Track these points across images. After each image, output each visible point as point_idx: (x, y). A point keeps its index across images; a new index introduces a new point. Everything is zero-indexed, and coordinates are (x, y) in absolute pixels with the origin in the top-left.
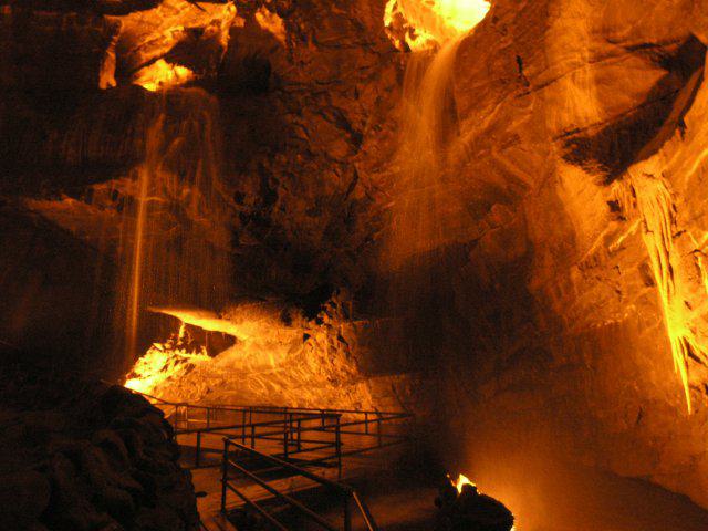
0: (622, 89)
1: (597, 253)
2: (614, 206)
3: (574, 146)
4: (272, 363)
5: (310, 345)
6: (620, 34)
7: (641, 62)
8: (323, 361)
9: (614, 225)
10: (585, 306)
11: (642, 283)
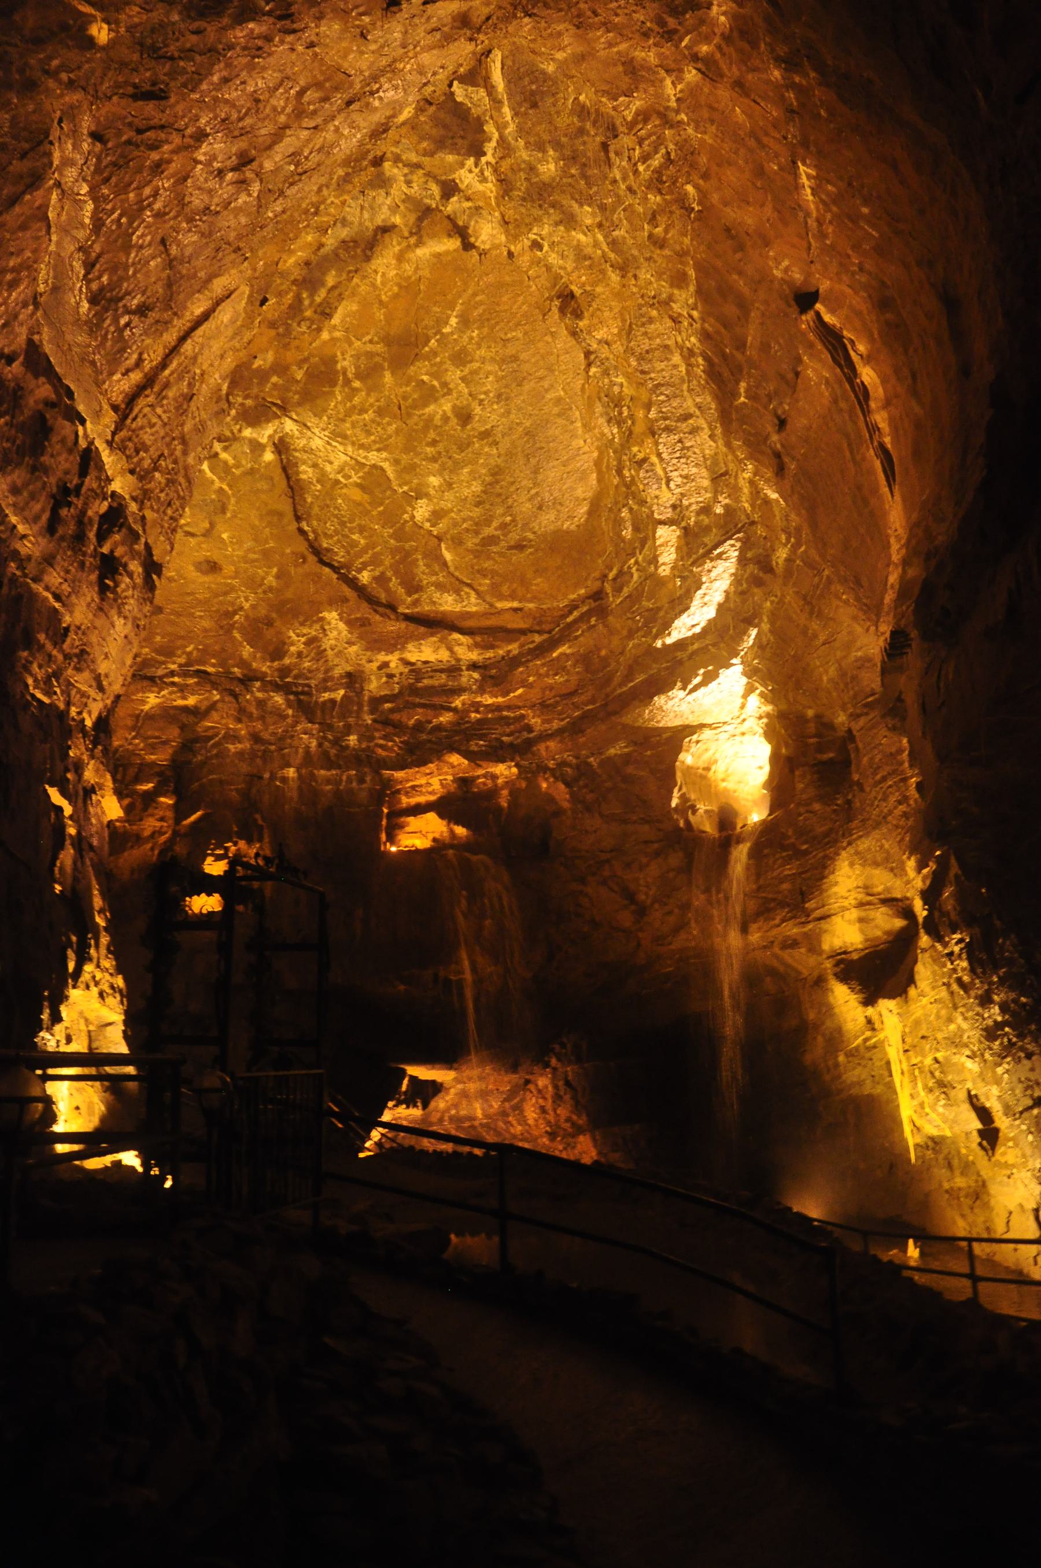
2: (869, 1021)
4: (479, 1114)
5: (531, 1092)
6: (876, 890)
7: (890, 912)
8: (543, 1110)
9: (868, 1034)
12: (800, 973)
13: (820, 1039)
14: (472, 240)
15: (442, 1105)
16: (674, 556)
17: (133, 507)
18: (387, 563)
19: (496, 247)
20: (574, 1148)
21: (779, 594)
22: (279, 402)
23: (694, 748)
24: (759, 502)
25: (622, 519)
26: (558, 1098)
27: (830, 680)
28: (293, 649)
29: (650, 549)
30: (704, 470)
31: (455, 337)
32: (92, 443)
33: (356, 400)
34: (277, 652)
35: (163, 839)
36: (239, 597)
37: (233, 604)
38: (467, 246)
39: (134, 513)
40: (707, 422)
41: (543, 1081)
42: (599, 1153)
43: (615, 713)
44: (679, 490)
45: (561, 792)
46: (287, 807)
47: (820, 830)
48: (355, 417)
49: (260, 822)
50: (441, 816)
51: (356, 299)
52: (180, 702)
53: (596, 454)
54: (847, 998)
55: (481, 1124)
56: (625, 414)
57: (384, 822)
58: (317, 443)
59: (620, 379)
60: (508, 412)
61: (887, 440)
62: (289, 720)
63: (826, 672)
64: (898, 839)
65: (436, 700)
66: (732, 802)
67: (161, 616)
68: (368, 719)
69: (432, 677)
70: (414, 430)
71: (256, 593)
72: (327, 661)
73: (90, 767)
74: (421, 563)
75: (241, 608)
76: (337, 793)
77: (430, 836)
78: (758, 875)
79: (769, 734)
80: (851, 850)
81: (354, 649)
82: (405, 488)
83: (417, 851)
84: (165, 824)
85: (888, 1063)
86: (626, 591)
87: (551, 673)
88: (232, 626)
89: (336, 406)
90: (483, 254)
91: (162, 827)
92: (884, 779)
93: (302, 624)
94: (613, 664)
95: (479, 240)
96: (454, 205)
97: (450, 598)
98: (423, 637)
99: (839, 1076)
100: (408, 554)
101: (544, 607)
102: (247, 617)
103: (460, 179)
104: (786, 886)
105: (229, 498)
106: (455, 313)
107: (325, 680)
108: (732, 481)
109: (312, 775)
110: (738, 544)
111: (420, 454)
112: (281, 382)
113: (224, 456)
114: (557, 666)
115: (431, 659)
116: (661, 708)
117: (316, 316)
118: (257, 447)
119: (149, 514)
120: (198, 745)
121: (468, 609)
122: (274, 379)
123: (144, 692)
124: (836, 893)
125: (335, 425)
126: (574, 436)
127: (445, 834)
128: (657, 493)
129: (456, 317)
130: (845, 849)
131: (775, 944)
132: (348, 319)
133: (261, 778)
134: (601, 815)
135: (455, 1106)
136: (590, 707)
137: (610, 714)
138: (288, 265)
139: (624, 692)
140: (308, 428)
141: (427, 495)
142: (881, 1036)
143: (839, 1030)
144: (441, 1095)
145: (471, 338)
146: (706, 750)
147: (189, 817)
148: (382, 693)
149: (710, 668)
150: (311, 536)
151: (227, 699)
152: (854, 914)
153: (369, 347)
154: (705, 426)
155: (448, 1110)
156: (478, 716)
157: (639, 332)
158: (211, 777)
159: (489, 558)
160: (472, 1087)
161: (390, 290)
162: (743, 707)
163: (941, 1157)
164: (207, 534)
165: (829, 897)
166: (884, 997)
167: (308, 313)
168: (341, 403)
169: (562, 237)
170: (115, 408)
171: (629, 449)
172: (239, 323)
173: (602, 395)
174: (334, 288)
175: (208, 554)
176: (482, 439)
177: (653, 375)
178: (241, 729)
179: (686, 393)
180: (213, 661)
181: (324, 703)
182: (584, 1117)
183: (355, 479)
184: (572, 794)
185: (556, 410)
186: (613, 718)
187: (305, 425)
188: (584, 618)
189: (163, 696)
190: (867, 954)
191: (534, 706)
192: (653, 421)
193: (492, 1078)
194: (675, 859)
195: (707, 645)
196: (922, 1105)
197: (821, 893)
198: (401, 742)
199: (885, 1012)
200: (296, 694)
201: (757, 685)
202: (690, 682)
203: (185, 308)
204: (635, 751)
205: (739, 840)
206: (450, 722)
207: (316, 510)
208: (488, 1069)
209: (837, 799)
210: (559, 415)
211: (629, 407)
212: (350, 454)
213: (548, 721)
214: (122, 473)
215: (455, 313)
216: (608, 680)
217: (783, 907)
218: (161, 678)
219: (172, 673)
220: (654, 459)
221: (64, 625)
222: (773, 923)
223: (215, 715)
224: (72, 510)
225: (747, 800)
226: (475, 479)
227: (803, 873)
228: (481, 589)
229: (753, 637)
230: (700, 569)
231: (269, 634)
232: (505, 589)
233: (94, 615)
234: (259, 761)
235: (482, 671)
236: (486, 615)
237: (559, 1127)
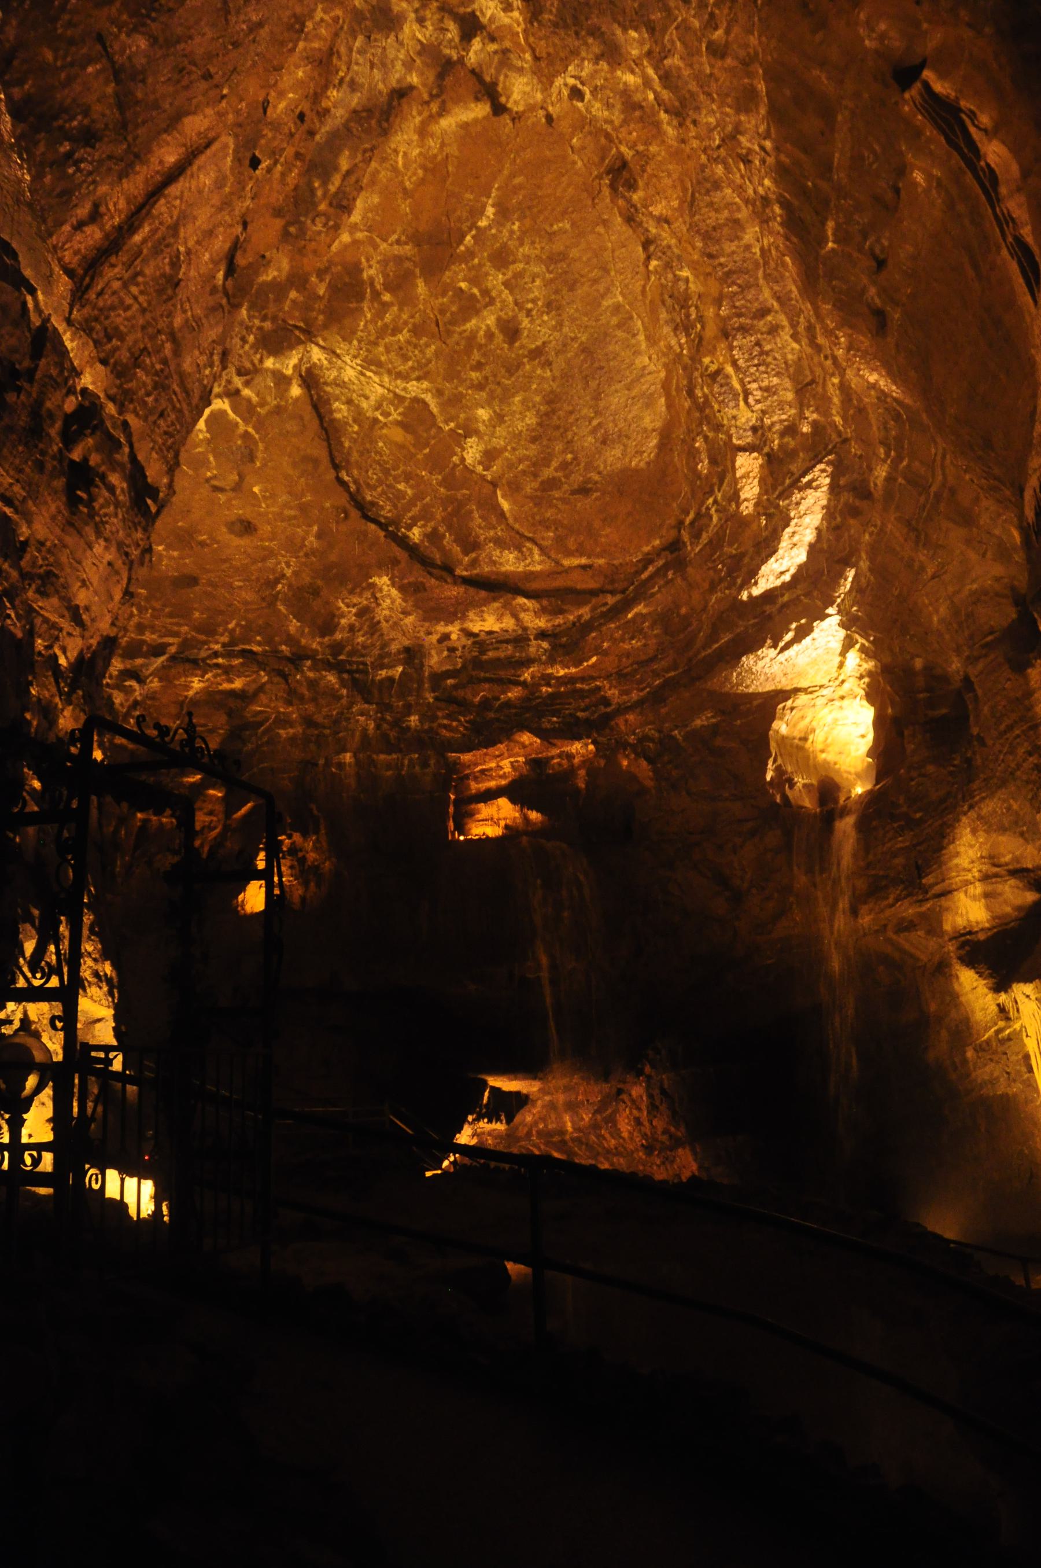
2: (1002, 1009)
5: (624, 1102)
6: (1003, 860)
7: (1021, 885)
8: (638, 1122)
9: (1001, 1024)
10: (979, 1081)
12: (918, 959)
13: (944, 1034)
14: (503, 100)
15: (529, 1119)
16: (756, 490)
17: (111, 408)
18: (438, 517)
19: (532, 108)
20: (672, 1162)
21: (879, 523)
22: (302, 324)
23: (788, 716)
24: (851, 412)
25: (697, 450)
26: (653, 1107)
27: (942, 621)
28: (343, 621)
29: (729, 485)
30: (787, 380)
31: (493, 231)
32: (47, 320)
33: (388, 318)
34: (327, 626)
35: (214, 833)
36: (279, 563)
37: (273, 571)
38: (499, 109)
39: (112, 417)
40: (788, 318)
41: (637, 1091)
42: (700, 1168)
43: (699, 678)
44: (759, 407)
46: (344, 795)
48: (388, 339)
49: (315, 812)
50: (513, 801)
51: (377, 188)
52: (226, 686)
53: (663, 374)
54: (975, 984)
56: (693, 317)
57: (451, 809)
58: (350, 374)
59: (685, 273)
60: (560, 325)
61: (1026, 233)
62: (344, 701)
63: (937, 611)
64: (1030, 796)
65: (502, 674)
66: (832, 775)
67: (197, 588)
69: (497, 649)
70: (455, 352)
71: (297, 557)
72: (382, 635)
73: (66, 713)
74: (476, 515)
75: (283, 576)
77: (502, 823)
79: (871, 696)
80: (973, 814)
81: (410, 620)
82: (452, 425)
84: (215, 819)
85: (1027, 1057)
86: (705, 538)
87: (627, 636)
88: (275, 597)
89: (365, 325)
90: (516, 118)
91: (212, 821)
92: (1010, 728)
93: (351, 592)
94: (695, 623)
95: (511, 100)
96: (477, 51)
97: (511, 556)
98: (486, 602)
99: (968, 1075)
100: (460, 505)
101: (616, 562)
102: (290, 586)
103: (481, 11)
104: (899, 861)
105: (256, 443)
106: (490, 201)
107: (381, 657)
108: (820, 389)
110: (829, 469)
111: (465, 380)
112: (302, 298)
113: (246, 392)
114: (634, 629)
116: (750, 670)
117: (331, 210)
118: (282, 380)
119: (131, 419)
120: (248, 733)
121: (531, 568)
122: (293, 294)
123: (187, 676)
124: (957, 865)
125: (368, 350)
126: (637, 353)
127: (518, 821)
128: (734, 412)
129: (493, 206)
130: (965, 814)
131: (889, 927)
132: (370, 215)
133: (316, 765)
135: (543, 1119)
136: (672, 674)
138: (278, 111)
140: (338, 356)
141: (476, 432)
142: (1017, 1026)
144: (526, 1108)
145: (512, 232)
146: (803, 717)
147: (240, 809)
148: (444, 669)
149: (803, 621)
150: (353, 487)
151: (277, 679)
152: (978, 889)
153: (397, 250)
154: (785, 323)
155: (536, 1123)
156: (550, 690)
157: (702, 200)
158: (261, 766)
159: (551, 506)
161: (415, 174)
162: (841, 665)
164: (237, 488)
165: (950, 869)
166: (1019, 981)
167: (322, 207)
168: (371, 321)
169: (606, 79)
170: (69, 272)
171: (701, 362)
172: (227, 189)
173: (666, 297)
174: (349, 173)
175: (241, 512)
176: (534, 359)
177: (722, 260)
178: (292, 712)
179: (761, 282)
180: (258, 638)
181: (382, 681)
182: (683, 1129)
183: (395, 416)
185: (614, 321)
187: (334, 352)
188: (661, 572)
189: (208, 680)
190: (998, 932)
191: (611, 675)
192: (725, 320)
195: (798, 597)
197: (940, 867)
199: (1021, 998)
200: (348, 672)
201: (857, 636)
202: (781, 638)
203: (150, 151)
205: (844, 812)
206: (518, 699)
207: (355, 456)
208: (576, 1079)
210: (619, 326)
211: (697, 307)
212: (387, 385)
213: (627, 693)
214: (90, 363)
215: (490, 201)
218: (204, 660)
219: (216, 655)
220: (729, 369)
221: (22, 539)
222: (885, 903)
223: (263, 698)
224: (22, 397)
225: (849, 773)
226: (528, 409)
227: (919, 844)
228: (545, 543)
229: (850, 579)
230: (787, 502)
231: (316, 604)
232: (571, 543)
233: (63, 530)
234: (313, 747)
235: (552, 639)
236: (550, 574)
237: (657, 1140)
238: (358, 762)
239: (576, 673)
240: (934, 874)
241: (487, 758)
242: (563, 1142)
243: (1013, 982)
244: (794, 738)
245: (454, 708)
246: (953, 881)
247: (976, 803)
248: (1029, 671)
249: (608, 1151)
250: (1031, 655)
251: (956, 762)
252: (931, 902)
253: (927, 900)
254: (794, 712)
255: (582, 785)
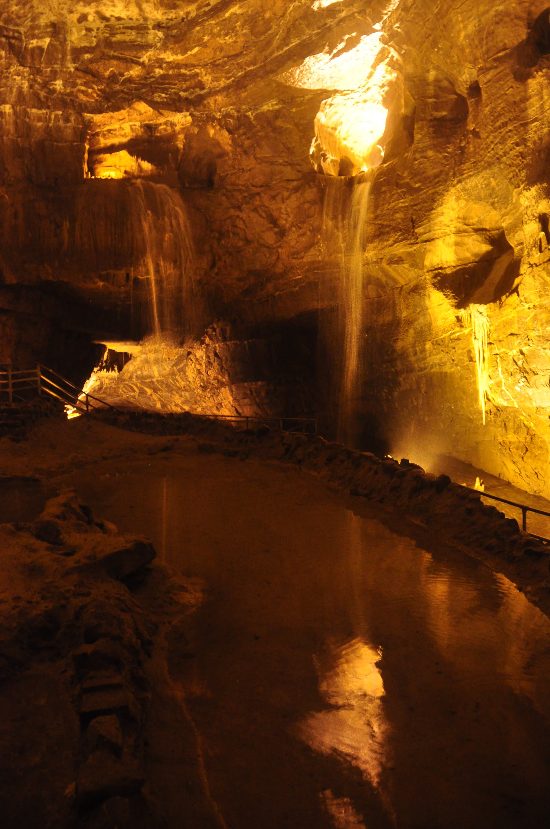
0: (468, 250)
1: (444, 338)
2: (459, 319)
3: (439, 278)
4: (156, 374)
5: (192, 360)
6: (471, 221)
7: (480, 239)
8: (199, 372)
9: (457, 329)
10: (431, 363)
11: (467, 360)
13: (411, 331)
23: (328, 110)
26: (209, 364)
41: (200, 353)
43: (272, 71)
45: (225, 138)
46: (5, 138)
47: (432, 172)
50: (131, 153)
54: (441, 303)
55: (157, 380)
57: (86, 156)
63: (465, 27)
65: (128, 54)
68: (71, 67)
69: (124, 33)
76: (47, 129)
77: (123, 169)
78: (376, 207)
79: (386, 101)
80: (459, 186)
83: (112, 179)
87: (223, 32)
92: (505, 124)
94: (274, 27)
99: (425, 358)
107: (32, 28)
109: (26, 114)
115: (123, 15)
124: (440, 222)
131: (383, 260)
134: (256, 158)
135: (140, 369)
136: (252, 68)
137: (267, 73)
139: (281, 55)
143: (429, 325)
144: (130, 362)
148: (83, 45)
149: (354, 34)
152: (452, 239)
160: (152, 357)
162: (370, 75)
163: (499, 420)
165: (435, 224)
181: (33, 49)
182: (227, 377)
184: (233, 140)
186: (271, 76)
190: (458, 270)
191: (207, 65)
193: (165, 351)
194: (310, 194)
196: (499, 384)
197: (429, 221)
198: (99, 90)
199: (474, 313)
204: (284, 108)
206: (138, 76)
209: (449, 148)
216: (269, 43)
217: (396, 231)
222: (386, 243)
225: (359, 156)
235: (165, 30)
238: (15, 112)
239: (182, 60)
240: (424, 227)
241: (113, 121)
242: (152, 382)
243: (471, 303)
244: (328, 127)
245: (89, 77)
246: (436, 232)
247: (464, 179)
248: (530, 81)
249: (179, 388)
250: (533, 69)
251: (449, 150)
252: (419, 245)
253: (417, 243)
254: (332, 107)
255: (181, 146)
